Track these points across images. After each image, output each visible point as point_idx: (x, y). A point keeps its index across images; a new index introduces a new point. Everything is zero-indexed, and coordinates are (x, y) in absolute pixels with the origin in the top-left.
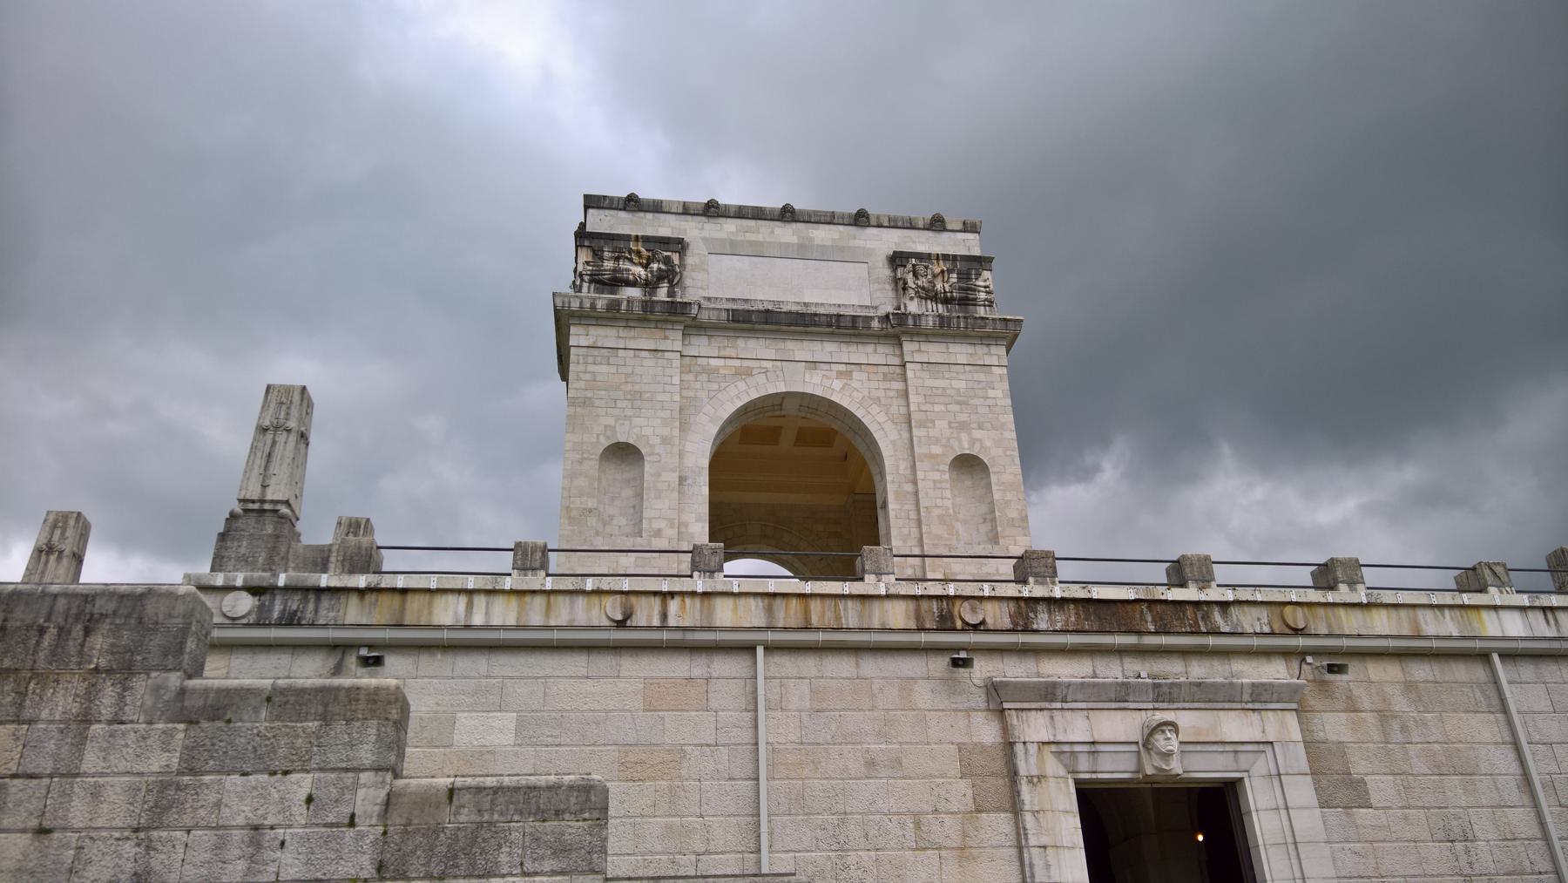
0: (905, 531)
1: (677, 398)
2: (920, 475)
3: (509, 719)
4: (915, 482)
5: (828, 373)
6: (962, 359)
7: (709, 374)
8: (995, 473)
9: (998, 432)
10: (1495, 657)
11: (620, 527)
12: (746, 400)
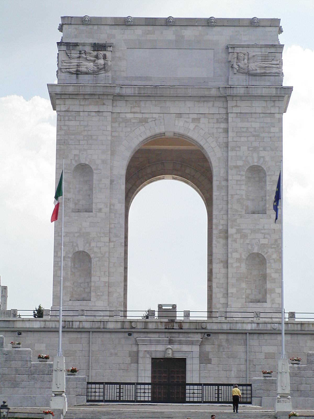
0: (220, 207)
1: (109, 138)
2: (230, 178)
3: (44, 345)
4: (227, 180)
5: (187, 120)
6: (259, 110)
7: (126, 123)
8: (269, 175)
9: (274, 152)
10: (248, 334)
11: (83, 205)
12: (144, 137)
